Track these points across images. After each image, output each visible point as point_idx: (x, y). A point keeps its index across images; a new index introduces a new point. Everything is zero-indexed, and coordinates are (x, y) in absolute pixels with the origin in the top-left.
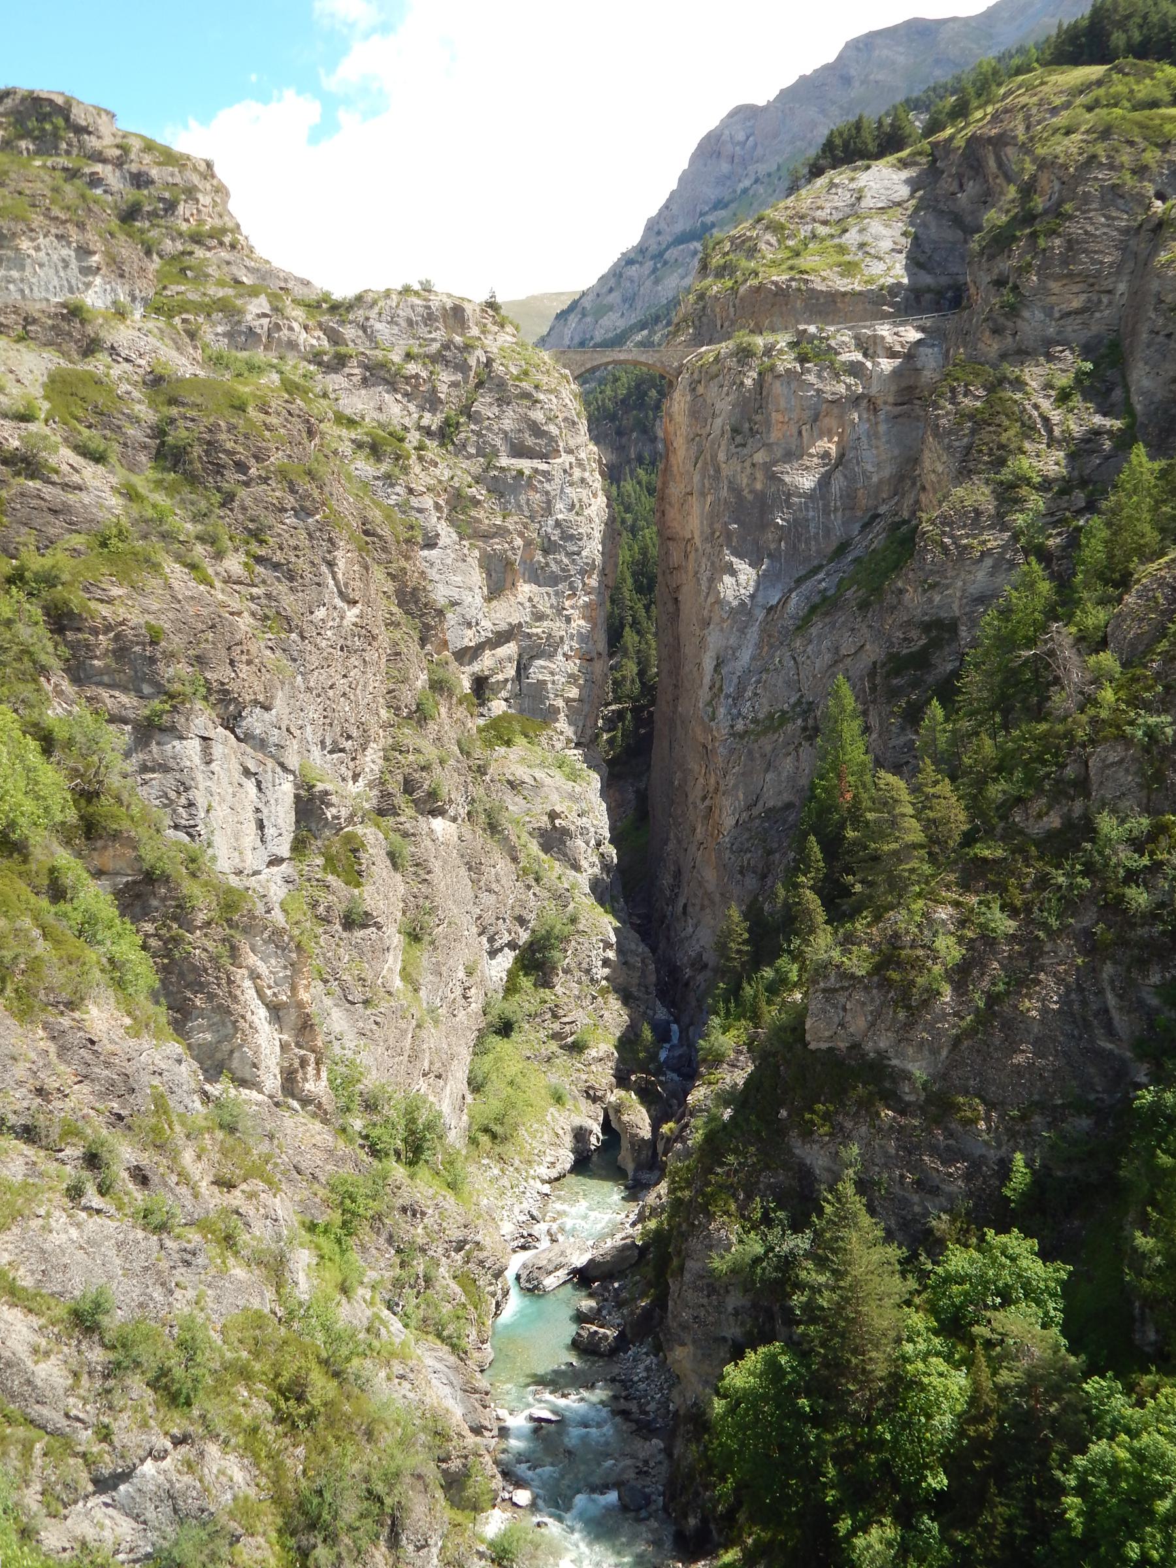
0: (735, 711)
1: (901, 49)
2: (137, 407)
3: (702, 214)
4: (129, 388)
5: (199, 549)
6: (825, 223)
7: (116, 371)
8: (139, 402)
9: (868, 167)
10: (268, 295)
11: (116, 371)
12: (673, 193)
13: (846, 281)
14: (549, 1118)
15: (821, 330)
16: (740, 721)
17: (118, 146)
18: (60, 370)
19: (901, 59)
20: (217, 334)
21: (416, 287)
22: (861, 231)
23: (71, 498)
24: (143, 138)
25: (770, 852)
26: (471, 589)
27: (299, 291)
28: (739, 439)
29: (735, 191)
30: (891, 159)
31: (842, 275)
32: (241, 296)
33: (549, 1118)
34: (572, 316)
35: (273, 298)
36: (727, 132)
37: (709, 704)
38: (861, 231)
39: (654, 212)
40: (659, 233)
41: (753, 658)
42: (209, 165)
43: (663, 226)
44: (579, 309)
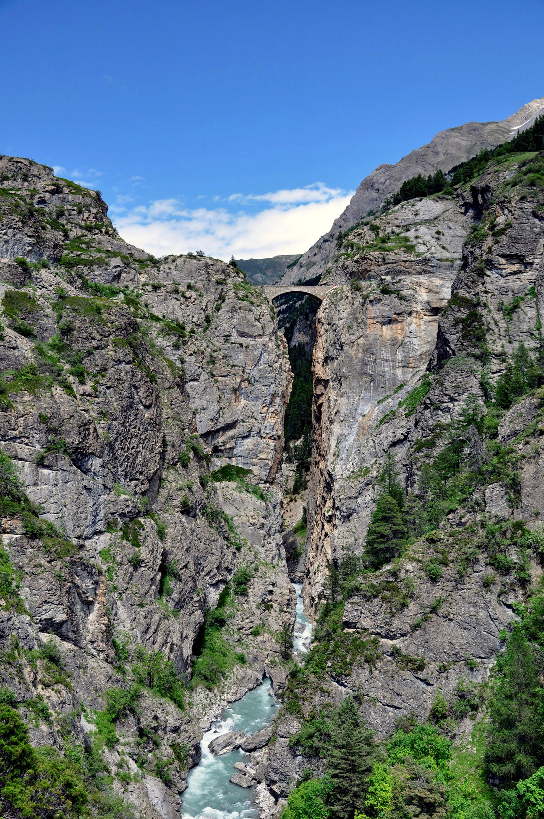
0: (344, 467)
1: (464, 138)
2: (47, 310)
3: (362, 218)
4: (44, 301)
5: (71, 379)
6: (398, 226)
7: (38, 292)
8: (49, 308)
9: (421, 200)
10: (121, 257)
11: (38, 292)
12: (348, 207)
13: (407, 255)
14: (235, 670)
15: (393, 279)
16: (346, 471)
17: (54, 185)
18: (10, 292)
19: (464, 143)
20: (357, 262)
21: (195, 254)
22: (417, 230)
23: (9, 353)
24: (65, 180)
25: (140, 443)
26: (213, 402)
27: (136, 256)
28: (351, 331)
29: (379, 207)
30: (433, 196)
31: (405, 252)
32: (109, 257)
33: (235, 670)
34: (295, 267)
35: (123, 258)
36: (375, 178)
37: (332, 463)
38: (417, 230)
39: (338, 216)
40: (340, 227)
41: (354, 440)
42: (98, 194)
43: (342, 223)
44: (299, 264)
